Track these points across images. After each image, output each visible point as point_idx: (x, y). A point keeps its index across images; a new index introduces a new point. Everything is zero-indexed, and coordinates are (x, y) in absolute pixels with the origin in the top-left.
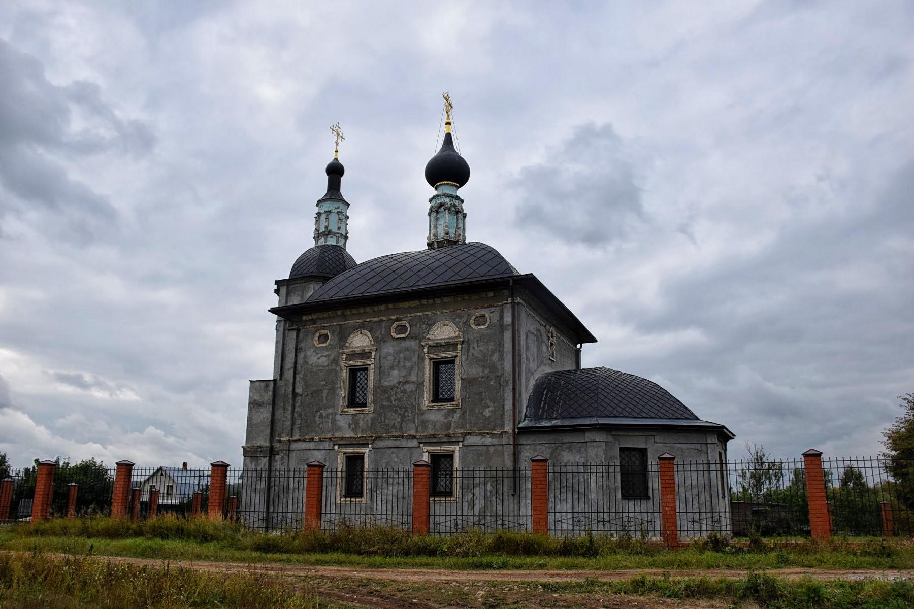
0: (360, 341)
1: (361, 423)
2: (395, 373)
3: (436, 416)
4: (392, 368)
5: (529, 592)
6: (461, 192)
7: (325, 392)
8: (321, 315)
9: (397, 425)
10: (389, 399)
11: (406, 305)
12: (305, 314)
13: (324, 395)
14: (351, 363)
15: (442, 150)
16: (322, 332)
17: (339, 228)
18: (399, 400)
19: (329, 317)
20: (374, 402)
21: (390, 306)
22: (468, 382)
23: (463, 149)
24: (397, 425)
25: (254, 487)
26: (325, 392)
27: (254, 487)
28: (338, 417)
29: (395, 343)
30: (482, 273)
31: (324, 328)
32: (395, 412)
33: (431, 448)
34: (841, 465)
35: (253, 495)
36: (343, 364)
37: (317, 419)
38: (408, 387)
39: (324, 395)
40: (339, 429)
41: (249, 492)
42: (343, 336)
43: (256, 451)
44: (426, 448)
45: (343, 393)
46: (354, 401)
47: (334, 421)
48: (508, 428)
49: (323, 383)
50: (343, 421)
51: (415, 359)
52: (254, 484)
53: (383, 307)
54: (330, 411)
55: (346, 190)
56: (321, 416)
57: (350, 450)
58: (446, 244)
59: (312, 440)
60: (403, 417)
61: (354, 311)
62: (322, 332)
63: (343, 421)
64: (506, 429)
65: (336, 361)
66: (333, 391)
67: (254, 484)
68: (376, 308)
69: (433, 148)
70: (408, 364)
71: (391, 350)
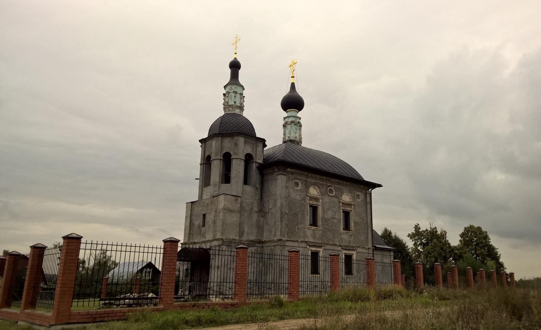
0: (313, 191)
1: (317, 235)
2: (330, 212)
3: (345, 236)
4: (328, 209)
5: (78, 328)
6: (300, 114)
7: (300, 215)
8: (296, 171)
9: (332, 239)
10: (328, 225)
11: (334, 180)
12: (290, 168)
13: (299, 217)
14: (311, 202)
15: (290, 92)
16: (297, 181)
17: (235, 102)
18: (332, 226)
19: (300, 174)
20: (322, 225)
21: (328, 178)
22: (356, 223)
23: (300, 91)
24: (332, 239)
25: (229, 266)
26: (300, 215)
27: (229, 266)
28: (306, 230)
29: (329, 197)
30: (356, 177)
31: (298, 179)
32: (331, 232)
33: (346, 252)
34: (99, 247)
35: (229, 272)
36: (308, 202)
37: (296, 229)
38: (335, 221)
39: (299, 217)
40: (307, 236)
41: (226, 270)
42: (307, 187)
43: (231, 242)
44: (344, 252)
45: (308, 218)
46: (314, 223)
47: (304, 233)
48: (370, 246)
49: (299, 210)
50: (309, 233)
51: (337, 208)
52: (229, 264)
53: (325, 178)
54: (302, 226)
55: (242, 79)
56: (298, 228)
57: (314, 249)
58: (292, 142)
59: (297, 241)
60: (334, 235)
61: (313, 175)
62: (297, 181)
63: (309, 233)
64: (370, 247)
65: (304, 199)
66: (303, 215)
67: (229, 264)
68: (322, 177)
69: (285, 91)
70: (335, 209)
71: (327, 200)
